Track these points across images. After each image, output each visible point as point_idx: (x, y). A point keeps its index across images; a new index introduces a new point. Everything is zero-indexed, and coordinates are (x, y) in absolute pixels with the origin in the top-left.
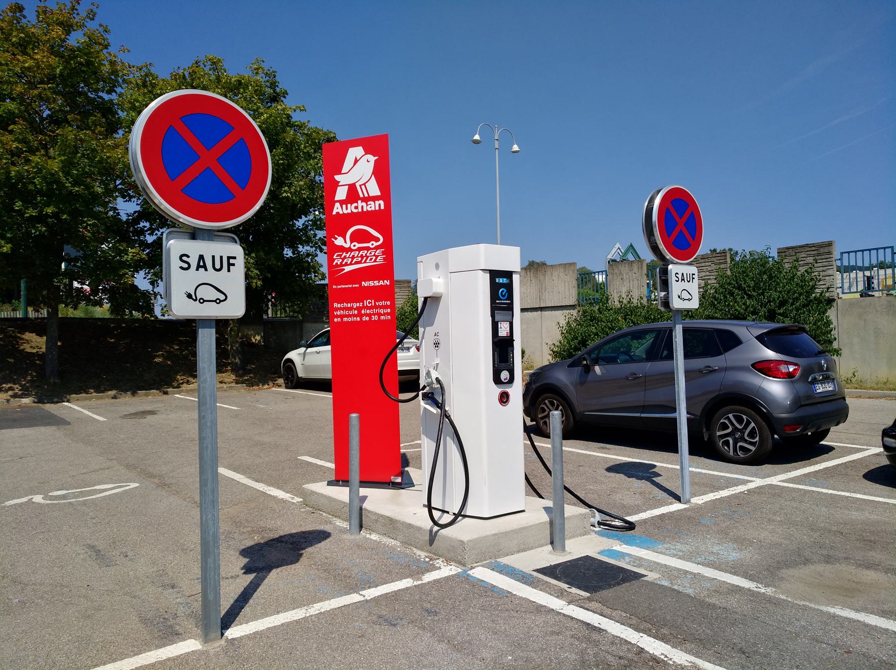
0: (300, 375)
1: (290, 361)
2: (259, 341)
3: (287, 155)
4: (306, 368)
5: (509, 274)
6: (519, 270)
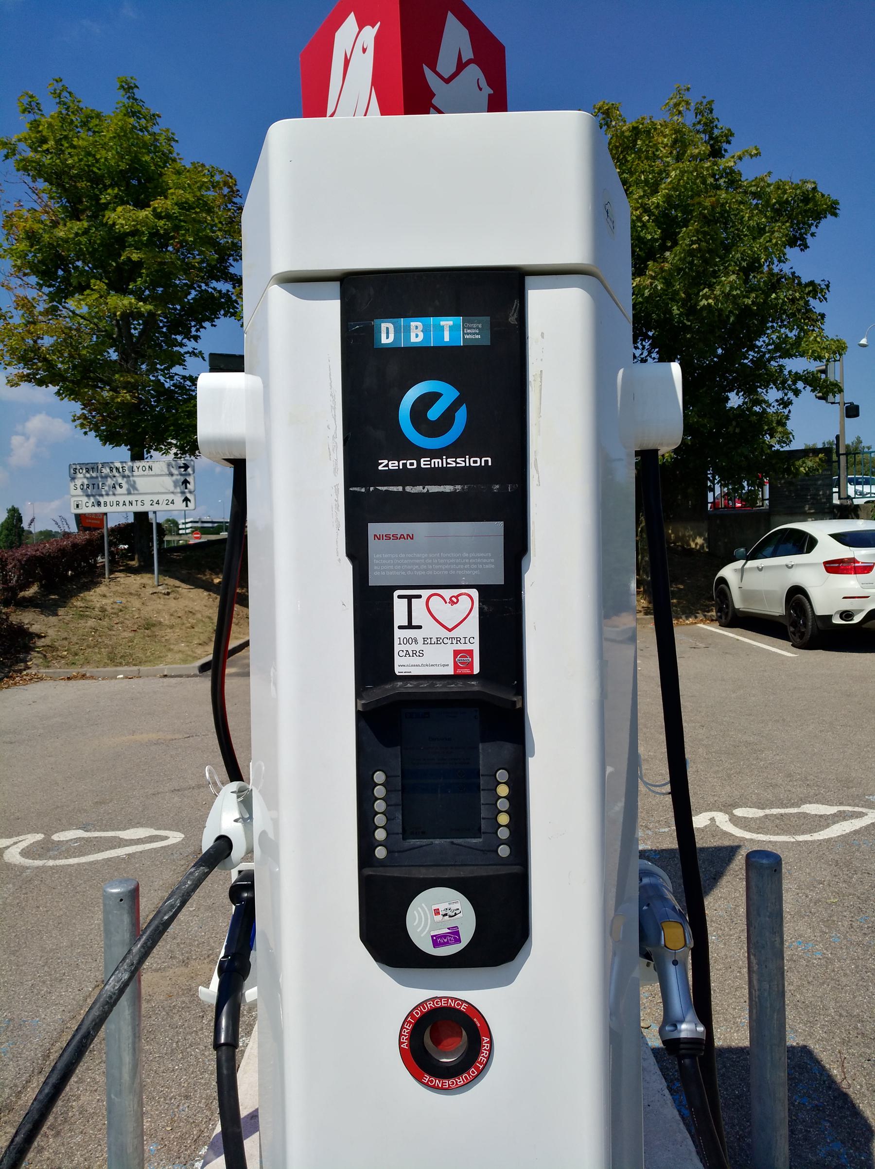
0: (737, 606)
1: (723, 581)
2: (702, 546)
3: (705, 234)
4: (747, 595)
5: (497, 293)
6: (570, 245)
